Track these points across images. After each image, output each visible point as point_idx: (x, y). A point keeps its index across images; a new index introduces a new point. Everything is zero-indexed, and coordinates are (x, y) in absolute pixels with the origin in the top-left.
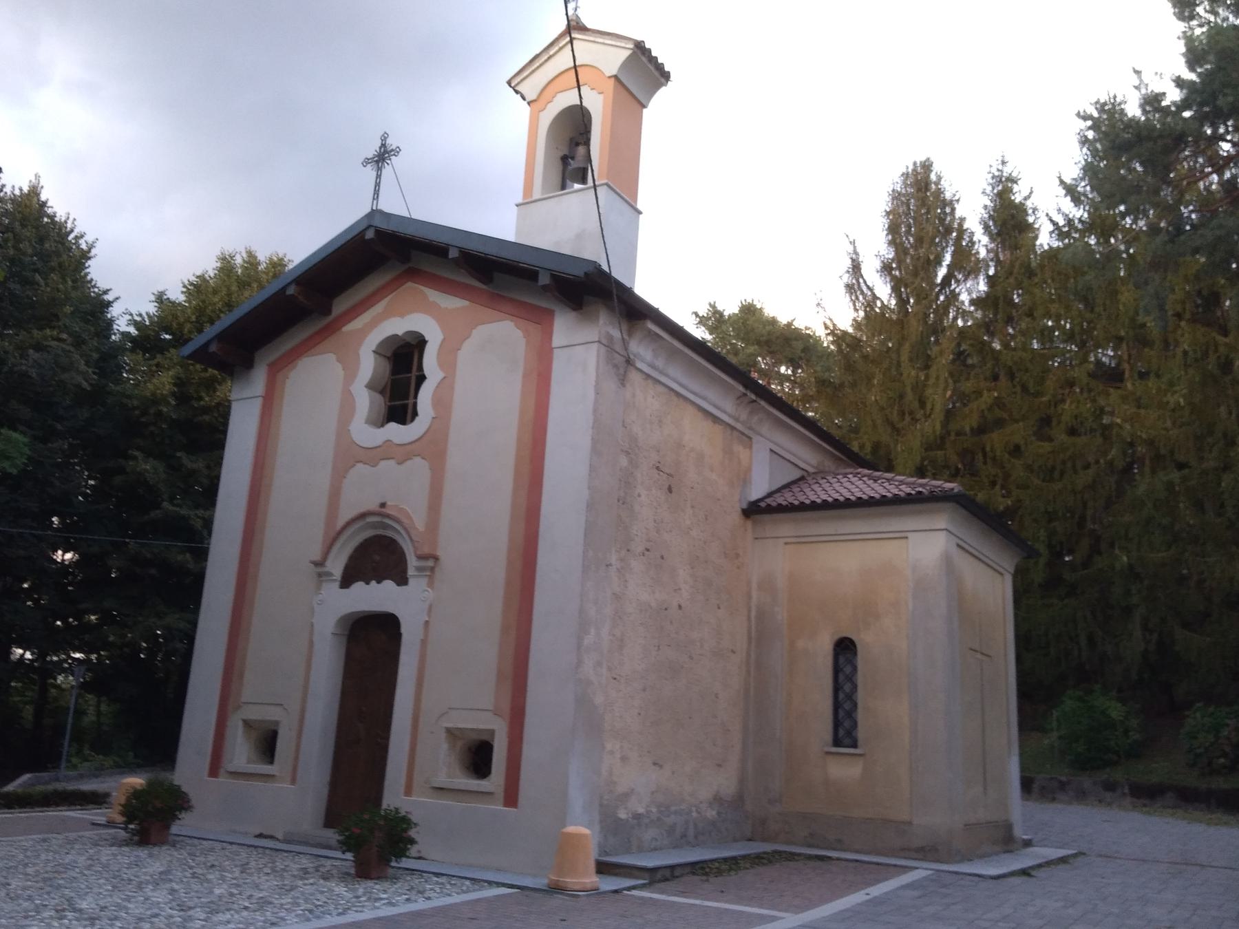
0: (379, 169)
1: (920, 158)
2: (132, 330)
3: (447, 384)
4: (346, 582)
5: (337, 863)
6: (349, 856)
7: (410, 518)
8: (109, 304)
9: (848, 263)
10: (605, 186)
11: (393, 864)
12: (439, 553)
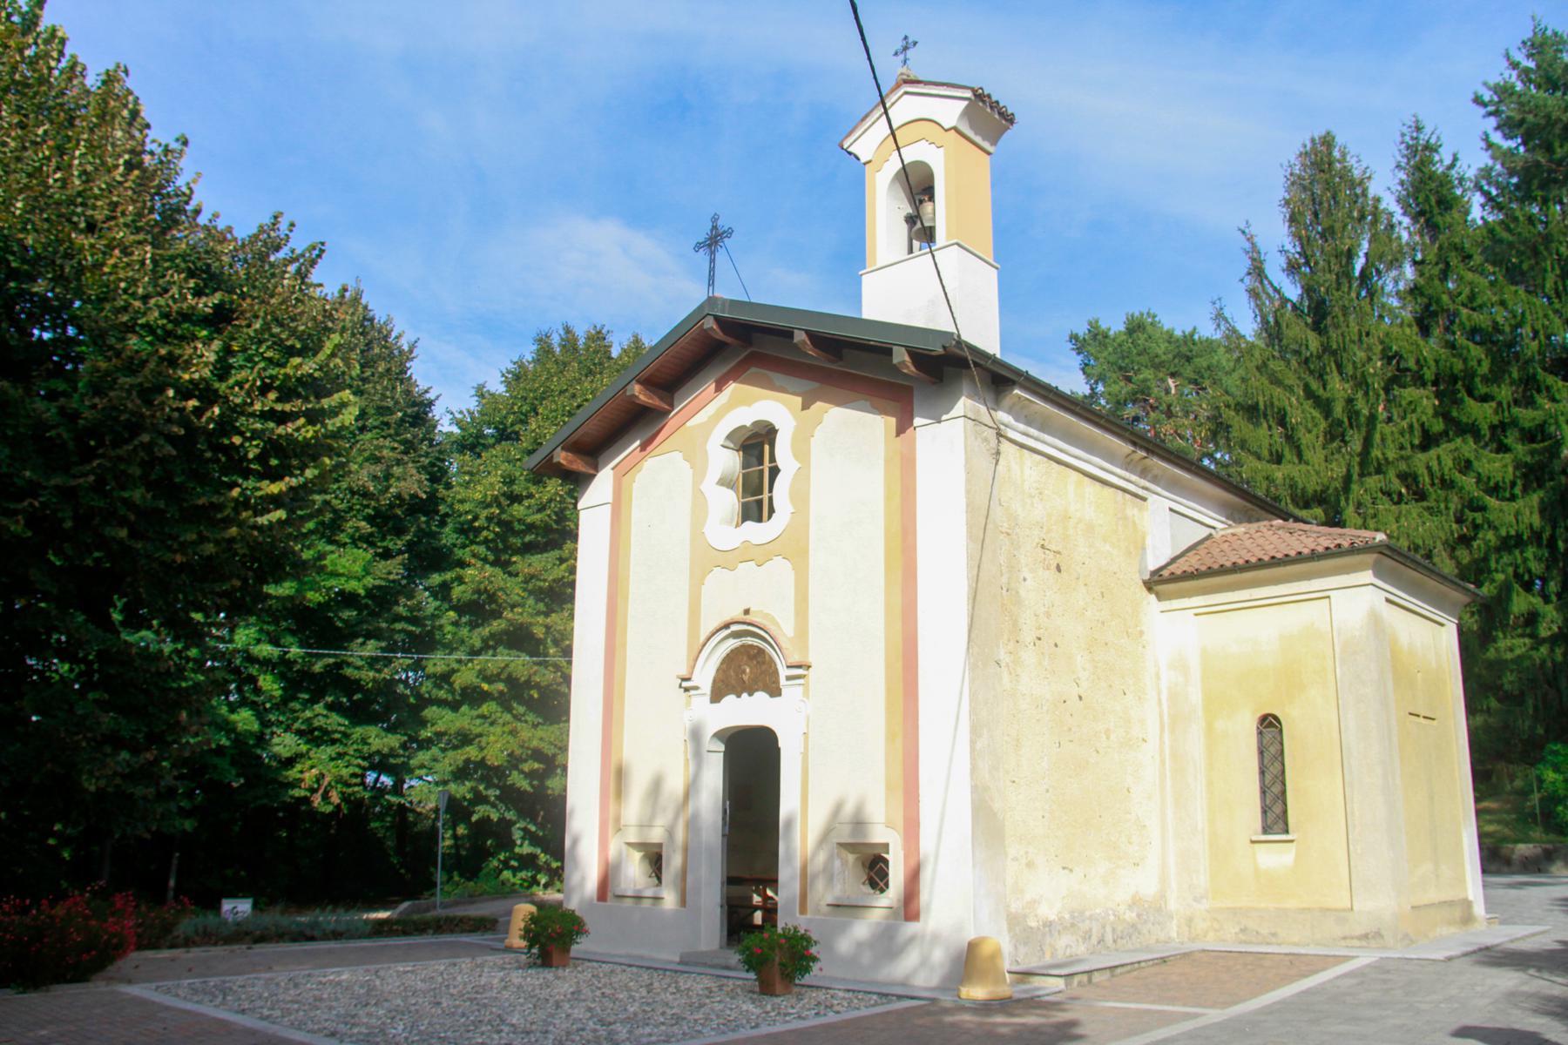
0: (713, 253)
1: (1318, 133)
2: (455, 430)
3: (803, 475)
4: (716, 696)
5: (740, 982)
6: (752, 975)
7: (777, 624)
8: (431, 403)
9: (1246, 263)
10: (905, 97)
11: (797, 981)
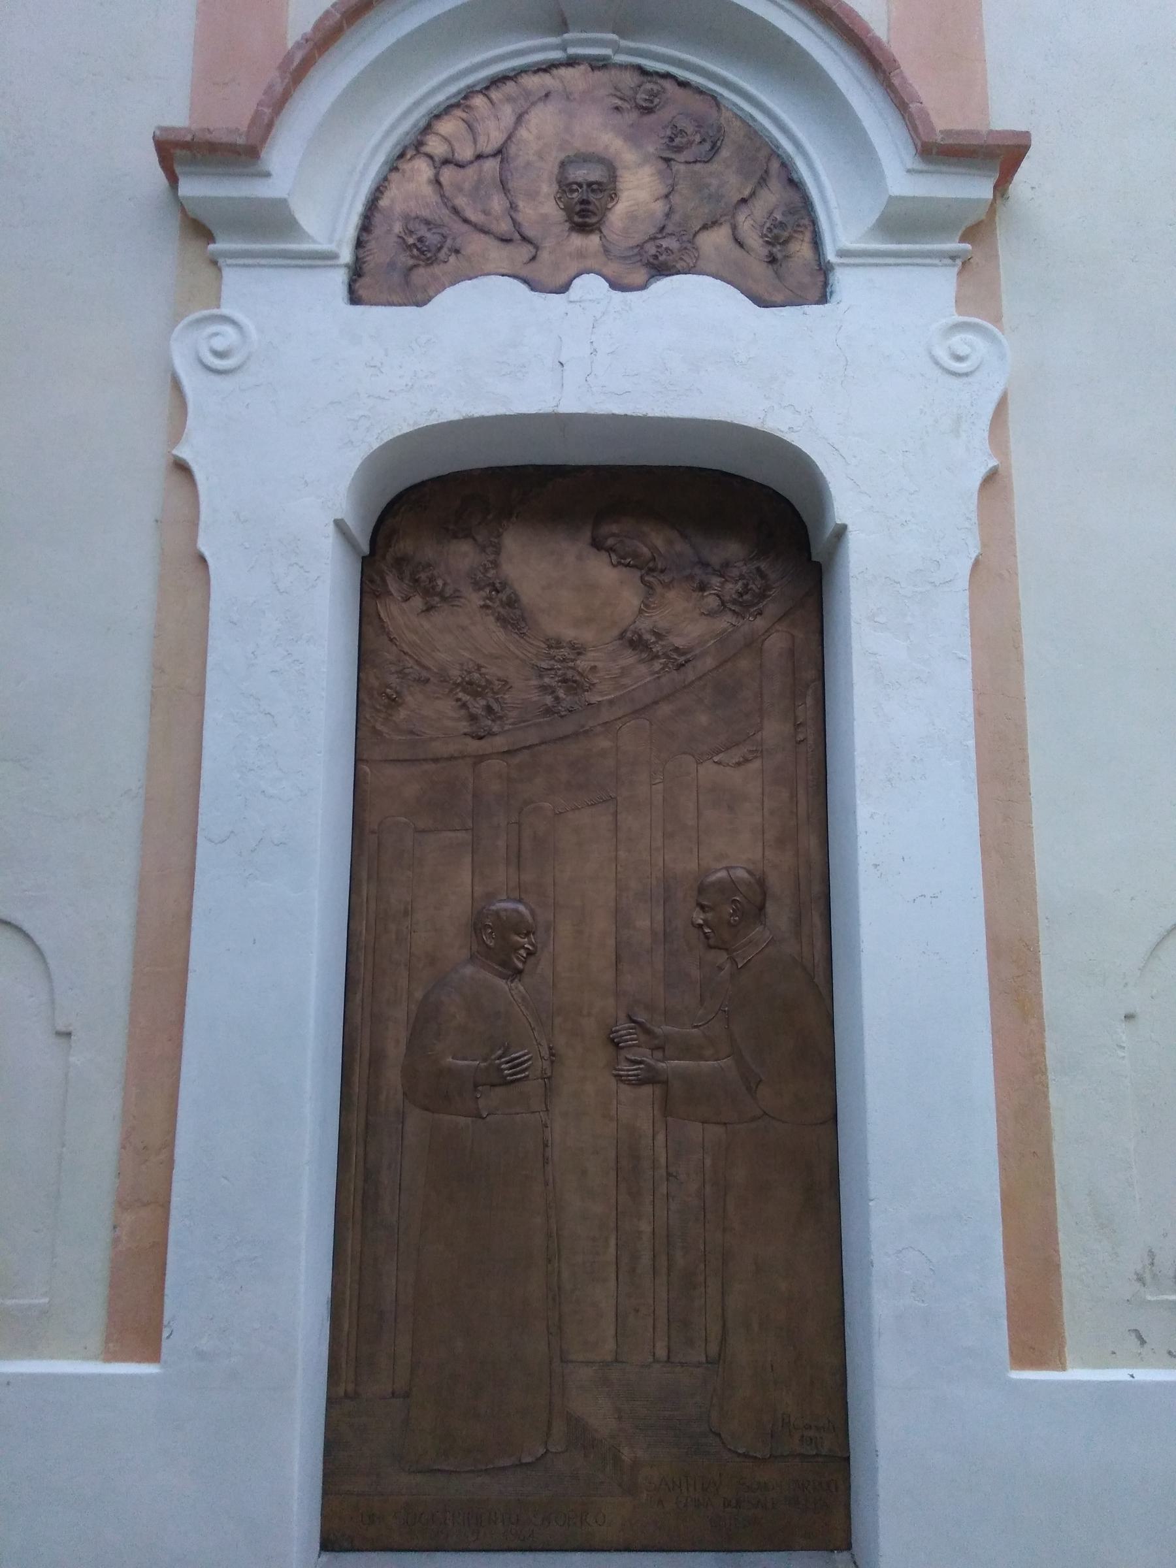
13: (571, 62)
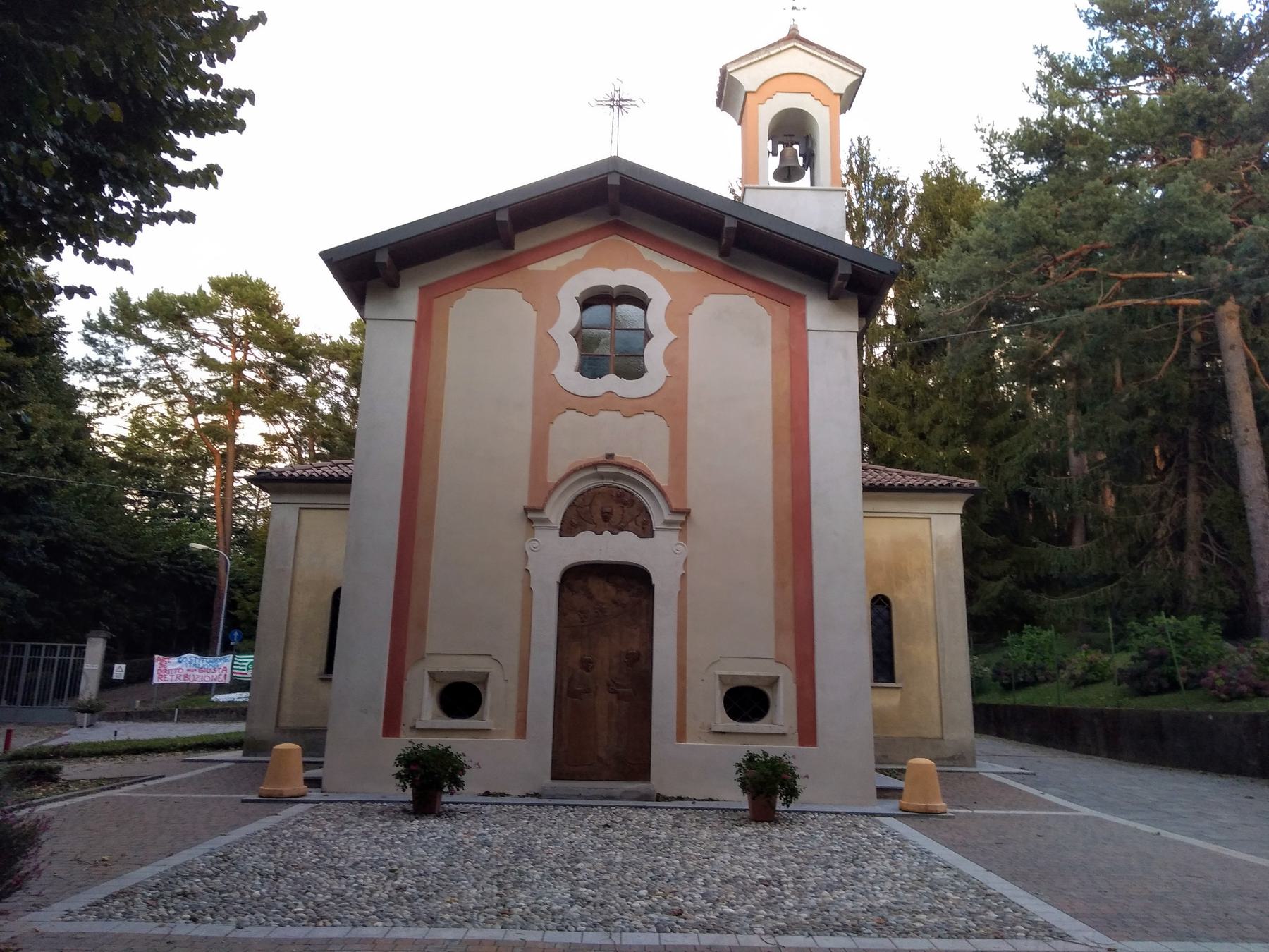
12: (690, 506)
13: (605, 485)
